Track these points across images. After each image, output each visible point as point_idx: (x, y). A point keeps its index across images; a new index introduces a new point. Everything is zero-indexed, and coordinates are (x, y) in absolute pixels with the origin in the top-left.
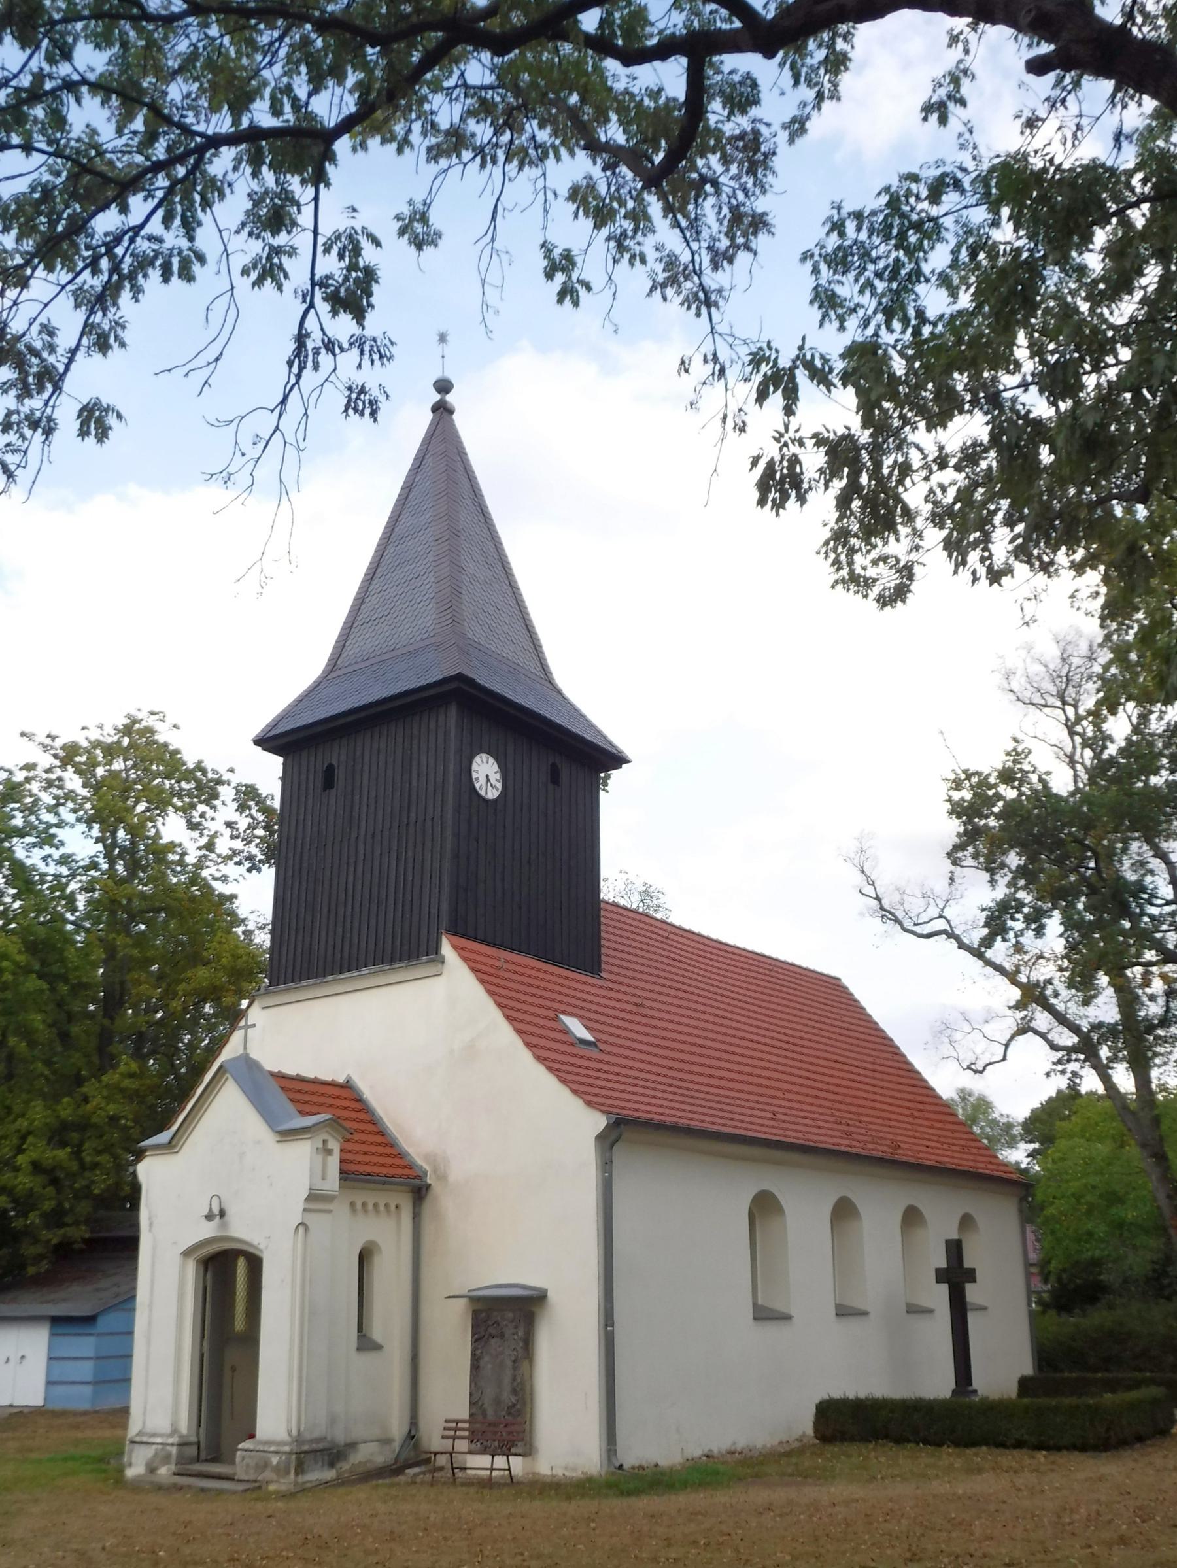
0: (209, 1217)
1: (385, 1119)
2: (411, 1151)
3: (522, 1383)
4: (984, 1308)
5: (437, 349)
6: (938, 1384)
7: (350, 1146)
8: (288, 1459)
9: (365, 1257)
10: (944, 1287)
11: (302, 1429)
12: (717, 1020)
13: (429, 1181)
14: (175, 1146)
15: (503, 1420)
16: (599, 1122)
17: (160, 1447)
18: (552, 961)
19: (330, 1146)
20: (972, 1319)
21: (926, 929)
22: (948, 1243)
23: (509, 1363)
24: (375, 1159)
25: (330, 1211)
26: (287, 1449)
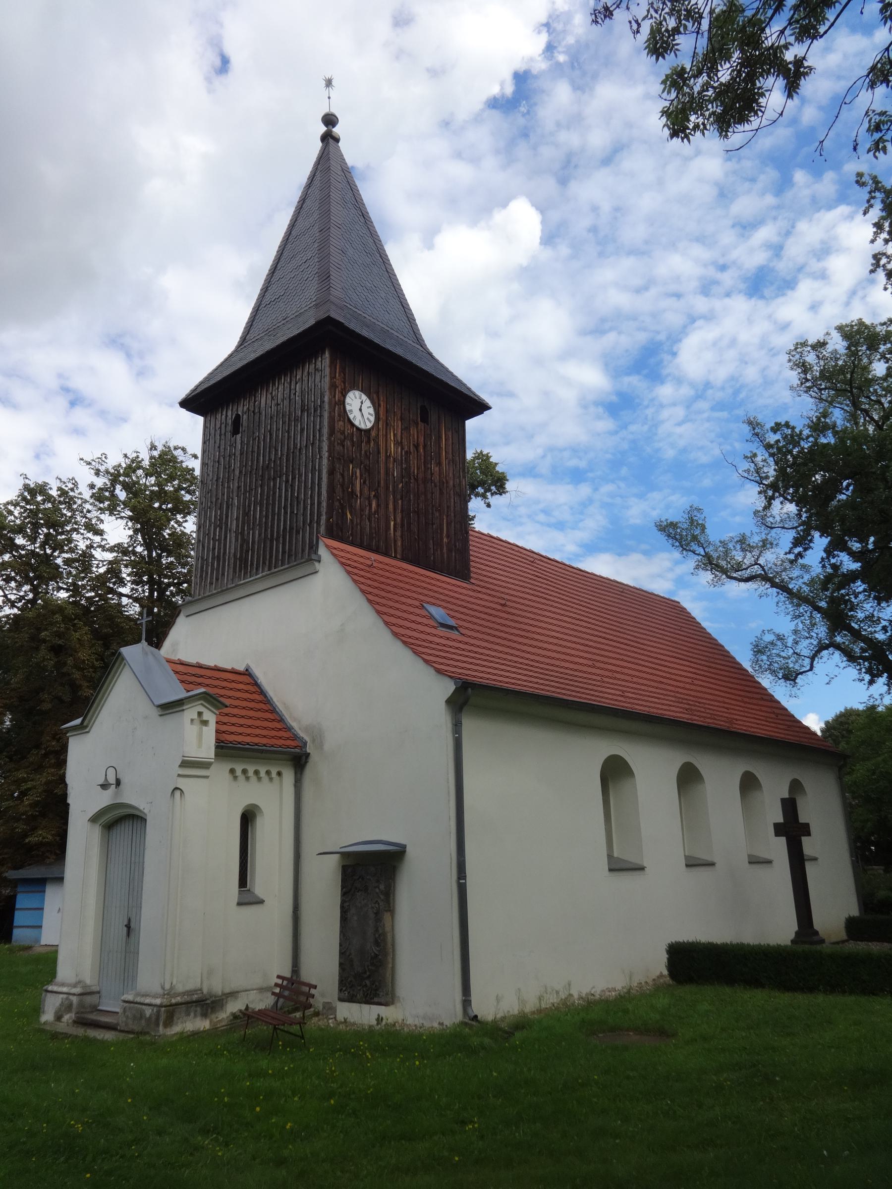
0: (105, 786)
1: (275, 700)
2: (294, 725)
3: (384, 934)
4: (815, 859)
5: (325, 92)
6: (778, 928)
7: (225, 719)
8: (158, 1012)
9: (248, 819)
10: (783, 840)
11: (174, 983)
12: (574, 621)
13: (308, 751)
14: (86, 727)
15: (367, 970)
16: (448, 688)
17: (65, 996)
18: (427, 567)
19: (205, 718)
20: (810, 868)
21: (746, 574)
22: (783, 801)
23: (372, 916)
24: (258, 731)
25: (207, 777)
26: (158, 1001)
